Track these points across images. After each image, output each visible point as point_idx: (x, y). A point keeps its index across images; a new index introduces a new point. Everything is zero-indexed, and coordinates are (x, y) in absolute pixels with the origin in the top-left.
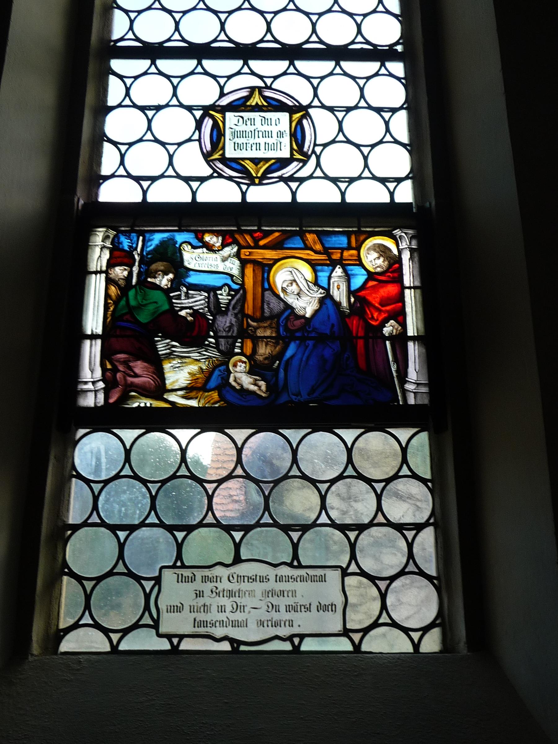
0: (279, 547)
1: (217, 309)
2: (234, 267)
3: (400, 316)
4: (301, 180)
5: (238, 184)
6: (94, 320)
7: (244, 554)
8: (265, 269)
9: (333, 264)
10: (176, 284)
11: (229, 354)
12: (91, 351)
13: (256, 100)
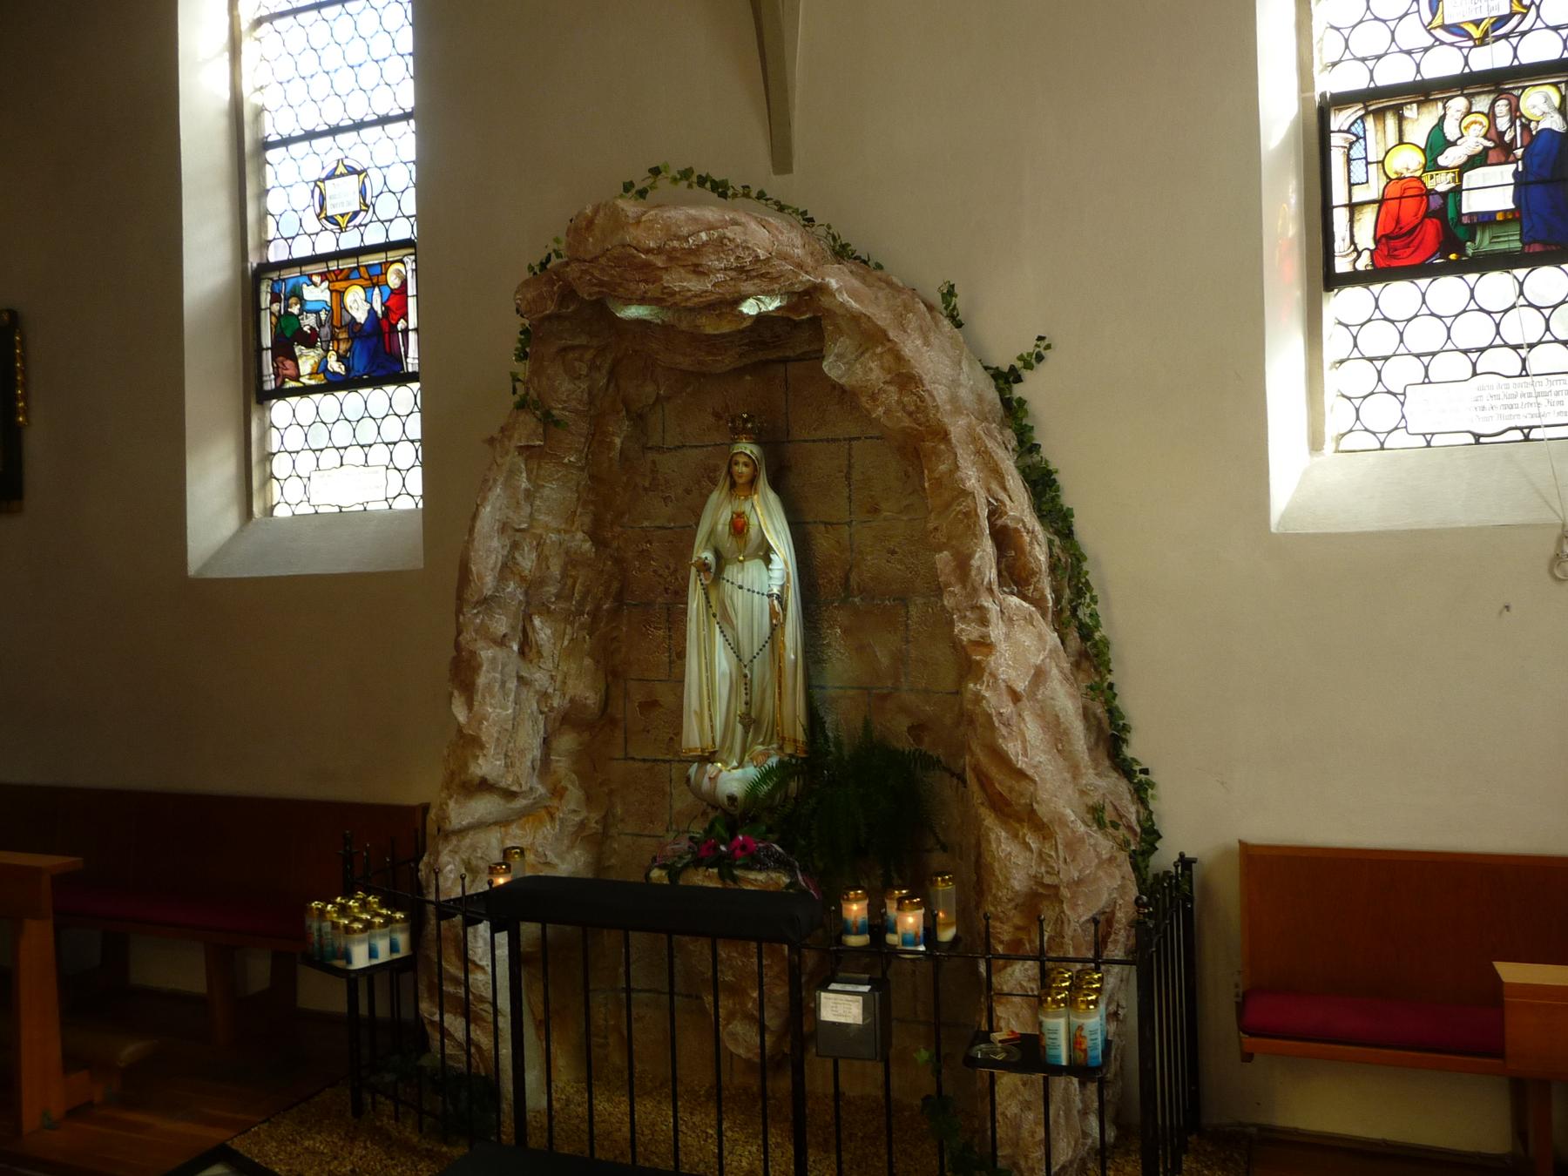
0: (1507, 361)
1: (320, 324)
2: (326, 296)
3: (405, 316)
4: (1523, 34)
5: (1460, 48)
6: (267, 341)
7: (1533, 367)
8: (341, 294)
9: (374, 286)
10: (302, 311)
11: (327, 351)
12: (267, 357)
13: (341, 169)
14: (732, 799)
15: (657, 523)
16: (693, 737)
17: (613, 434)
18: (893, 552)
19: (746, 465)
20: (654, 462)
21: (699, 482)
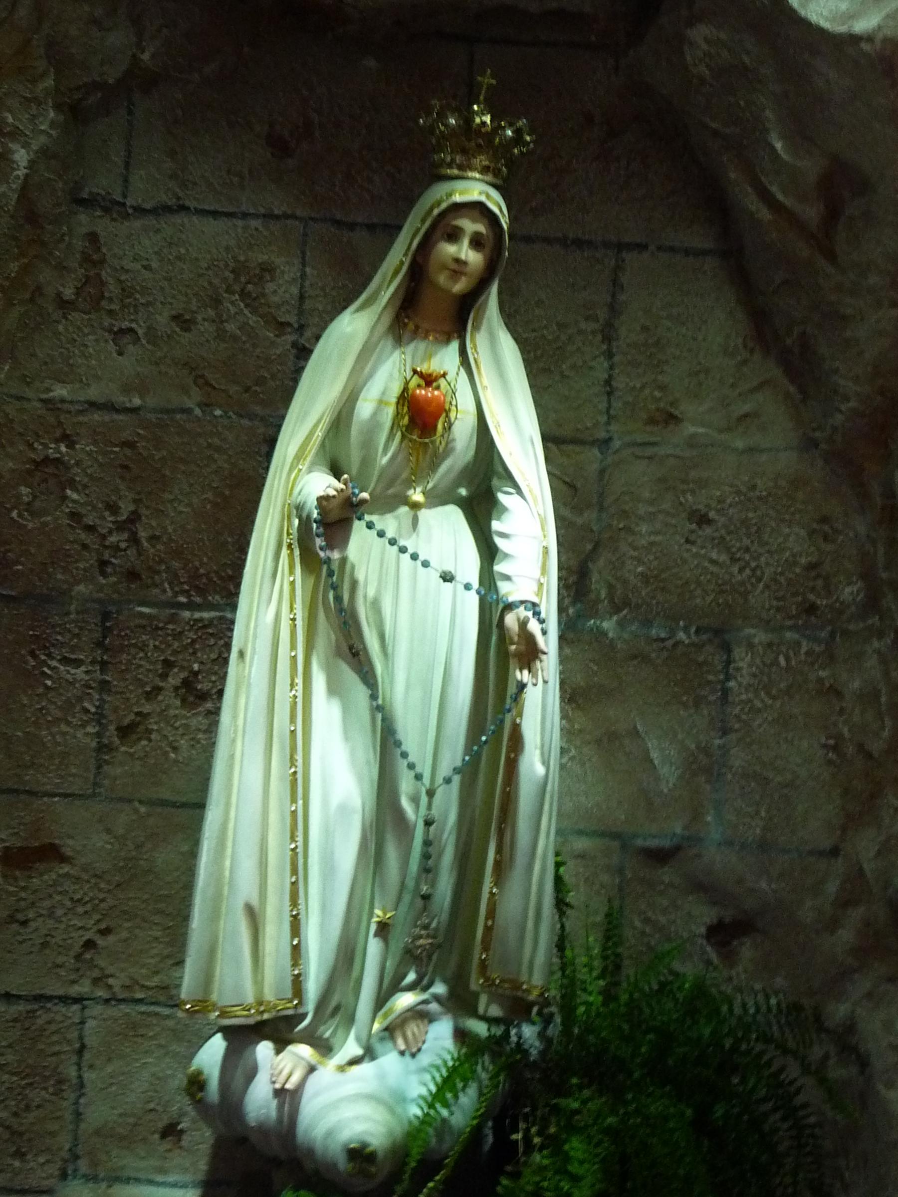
14: (359, 1154)
15: (93, 393)
16: (237, 969)
17: (15, 134)
18: (703, 520)
19: (477, 242)
20: (93, 238)
21: (216, 302)
